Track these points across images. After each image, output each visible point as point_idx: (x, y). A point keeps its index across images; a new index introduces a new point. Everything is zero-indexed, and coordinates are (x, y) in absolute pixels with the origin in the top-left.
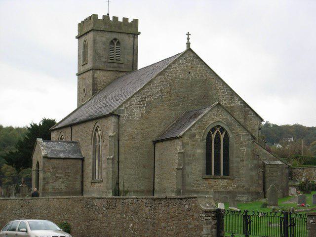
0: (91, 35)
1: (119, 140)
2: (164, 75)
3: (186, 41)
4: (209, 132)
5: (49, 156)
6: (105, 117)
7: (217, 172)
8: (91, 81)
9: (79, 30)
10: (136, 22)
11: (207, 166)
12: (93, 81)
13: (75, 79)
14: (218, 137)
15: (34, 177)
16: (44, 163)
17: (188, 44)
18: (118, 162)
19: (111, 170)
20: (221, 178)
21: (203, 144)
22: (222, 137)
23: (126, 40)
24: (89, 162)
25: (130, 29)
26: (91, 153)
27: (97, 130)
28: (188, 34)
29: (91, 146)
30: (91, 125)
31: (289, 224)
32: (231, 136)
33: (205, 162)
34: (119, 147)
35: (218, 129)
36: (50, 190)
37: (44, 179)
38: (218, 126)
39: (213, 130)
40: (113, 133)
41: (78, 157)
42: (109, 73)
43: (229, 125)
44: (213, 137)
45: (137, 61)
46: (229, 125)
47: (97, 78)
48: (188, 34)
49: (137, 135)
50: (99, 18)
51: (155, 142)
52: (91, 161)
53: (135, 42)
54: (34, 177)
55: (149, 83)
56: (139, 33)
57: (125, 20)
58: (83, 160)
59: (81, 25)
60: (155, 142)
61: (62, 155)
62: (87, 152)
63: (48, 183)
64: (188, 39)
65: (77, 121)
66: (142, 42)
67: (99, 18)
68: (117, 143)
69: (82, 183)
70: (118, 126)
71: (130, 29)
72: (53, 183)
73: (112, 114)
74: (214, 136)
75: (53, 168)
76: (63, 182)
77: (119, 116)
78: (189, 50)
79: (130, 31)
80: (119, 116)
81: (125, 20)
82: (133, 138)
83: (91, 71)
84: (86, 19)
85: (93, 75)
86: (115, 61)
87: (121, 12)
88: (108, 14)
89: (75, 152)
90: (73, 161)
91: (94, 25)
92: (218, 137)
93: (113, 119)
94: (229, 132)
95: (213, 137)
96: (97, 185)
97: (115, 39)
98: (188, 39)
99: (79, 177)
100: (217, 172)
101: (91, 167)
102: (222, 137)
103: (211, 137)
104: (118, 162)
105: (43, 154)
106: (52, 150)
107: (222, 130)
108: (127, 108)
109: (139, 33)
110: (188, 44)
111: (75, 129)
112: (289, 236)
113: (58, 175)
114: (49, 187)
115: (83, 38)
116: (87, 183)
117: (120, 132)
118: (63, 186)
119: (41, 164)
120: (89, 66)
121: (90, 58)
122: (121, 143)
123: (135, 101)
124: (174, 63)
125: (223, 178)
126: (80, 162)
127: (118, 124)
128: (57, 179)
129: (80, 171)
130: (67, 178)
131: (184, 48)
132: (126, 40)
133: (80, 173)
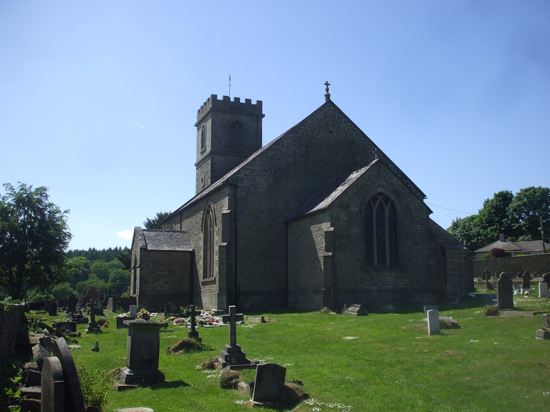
3: (325, 93)
4: (369, 203)
9: (198, 115)
10: (260, 103)
13: (193, 170)
14: (381, 209)
17: (328, 96)
18: (236, 251)
19: (225, 262)
22: (387, 210)
25: (252, 113)
26: (201, 243)
28: (327, 84)
29: (202, 235)
31: (138, 270)
32: (398, 207)
34: (236, 229)
35: (381, 198)
38: (381, 194)
40: (229, 209)
44: (375, 209)
52: (202, 253)
56: (264, 116)
60: (287, 224)
64: (327, 90)
66: (265, 122)
71: (252, 113)
72: (153, 283)
74: (376, 207)
78: (329, 102)
84: (205, 103)
87: (241, 92)
92: (381, 209)
95: (375, 209)
97: (237, 122)
98: (327, 90)
104: (236, 251)
107: (387, 199)
108: (247, 176)
109: (264, 116)
110: (328, 96)
130: (171, 277)
131: (323, 101)
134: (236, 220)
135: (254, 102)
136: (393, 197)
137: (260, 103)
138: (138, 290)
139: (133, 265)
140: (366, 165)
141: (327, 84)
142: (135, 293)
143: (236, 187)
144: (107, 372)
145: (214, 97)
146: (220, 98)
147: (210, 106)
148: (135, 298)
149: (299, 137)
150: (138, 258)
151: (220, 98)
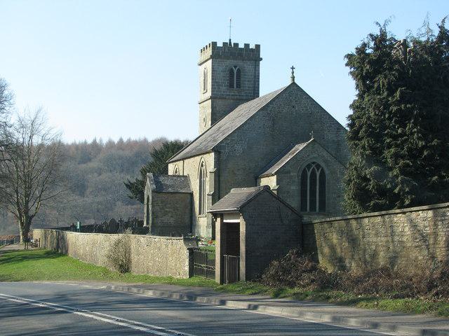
4: (305, 169)
7: (313, 208)
10: (258, 47)
11: (302, 203)
14: (313, 174)
17: (293, 78)
20: (316, 214)
21: (297, 180)
22: (318, 174)
23: (248, 67)
25: (252, 55)
27: (202, 166)
28: (293, 68)
30: (198, 158)
32: (327, 172)
33: (299, 198)
38: (314, 163)
39: (309, 166)
41: (186, 191)
43: (326, 162)
44: (309, 174)
45: (259, 88)
46: (326, 162)
47: (216, 107)
50: (218, 46)
56: (261, 59)
64: (293, 73)
67: (218, 46)
71: (252, 55)
78: (294, 84)
82: (234, 174)
88: (230, 40)
92: (313, 174)
94: (325, 169)
95: (309, 174)
98: (293, 73)
100: (313, 208)
102: (318, 174)
103: (307, 174)
107: (318, 166)
109: (261, 59)
110: (293, 78)
111: (186, 161)
112: (2, 249)
113: (167, 210)
118: (172, 220)
125: (318, 214)
126: (189, 196)
128: (166, 214)
131: (289, 82)
132: (248, 67)
134: (219, 176)
135: (252, 46)
136: (323, 165)
137: (258, 47)
138: (150, 222)
139: (146, 201)
140: (304, 142)
141: (293, 68)
142: (148, 223)
143: (220, 152)
144: (360, 213)
145: (214, 44)
146: (220, 44)
147: (209, 52)
148: (148, 228)
149: (268, 113)
150: (151, 198)
151: (220, 44)
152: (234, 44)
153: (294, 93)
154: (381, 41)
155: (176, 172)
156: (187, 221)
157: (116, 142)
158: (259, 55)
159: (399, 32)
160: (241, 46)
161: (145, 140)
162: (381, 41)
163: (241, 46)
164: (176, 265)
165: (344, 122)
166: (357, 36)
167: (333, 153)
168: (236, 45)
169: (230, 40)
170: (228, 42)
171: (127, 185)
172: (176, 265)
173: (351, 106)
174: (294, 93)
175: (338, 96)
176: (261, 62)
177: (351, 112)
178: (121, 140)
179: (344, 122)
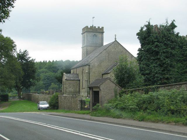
0: (86, 33)
1: (89, 74)
2: (106, 50)
5: (67, 79)
6: (85, 65)
8: (86, 50)
10: (103, 28)
12: (86, 50)
15: (63, 88)
16: (66, 82)
17: (115, 39)
18: (89, 82)
24: (81, 81)
26: (82, 78)
27: (83, 70)
28: (115, 35)
30: (82, 68)
36: (68, 91)
37: (66, 87)
42: (92, 47)
48: (115, 35)
49: (96, 72)
51: (103, 75)
52: (82, 81)
53: (103, 35)
54: (63, 88)
55: (101, 53)
57: (99, 27)
58: (79, 80)
59: (83, 29)
61: (72, 79)
62: (80, 78)
63: (67, 89)
65: (78, 66)
68: (89, 75)
69: (79, 89)
70: (89, 69)
73: (87, 65)
75: (69, 83)
76: (72, 88)
77: (89, 65)
78: (116, 41)
79: (101, 31)
80: (89, 65)
81: (99, 27)
83: (86, 47)
85: (87, 48)
86: (95, 43)
88: (93, 25)
89: (77, 78)
90: (76, 81)
91: (87, 30)
93: (88, 67)
96: (83, 90)
98: (115, 37)
99: (78, 86)
101: (82, 83)
104: (89, 82)
105: (65, 79)
106: (69, 77)
110: (115, 39)
114: (68, 90)
115: (84, 34)
116: (81, 89)
117: (90, 71)
119: (65, 81)
120: (85, 45)
121: (85, 42)
122: (90, 75)
123: (95, 60)
124: (110, 46)
126: (78, 81)
127: (89, 68)
129: (79, 84)
131: (114, 40)
132: (99, 35)
133: (79, 85)
137: (103, 28)
152: (94, 27)
153: (116, 43)
154: (149, 26)
155: (74, 72)
156: (78, 90)
157: (55, 61)
158: (103, 30)
159: (153, 23)
160: (97, 27)
161: (62, 61)
162: (149, 26)
163: (97, 27)
164: (75, 106)
165: (136, 55)
166: (140, 24)
167: (132, 109)
168: (95, 27)
169: (93, 25)
170: (92, 26)
171: (56, 78)
172: (75, 106)
173: (138, 50)
174: (116, 43)
175: (133, 48)
176: (104, 33)
177: (138, 52)
178: (53, 61)
179: (105, 44)
